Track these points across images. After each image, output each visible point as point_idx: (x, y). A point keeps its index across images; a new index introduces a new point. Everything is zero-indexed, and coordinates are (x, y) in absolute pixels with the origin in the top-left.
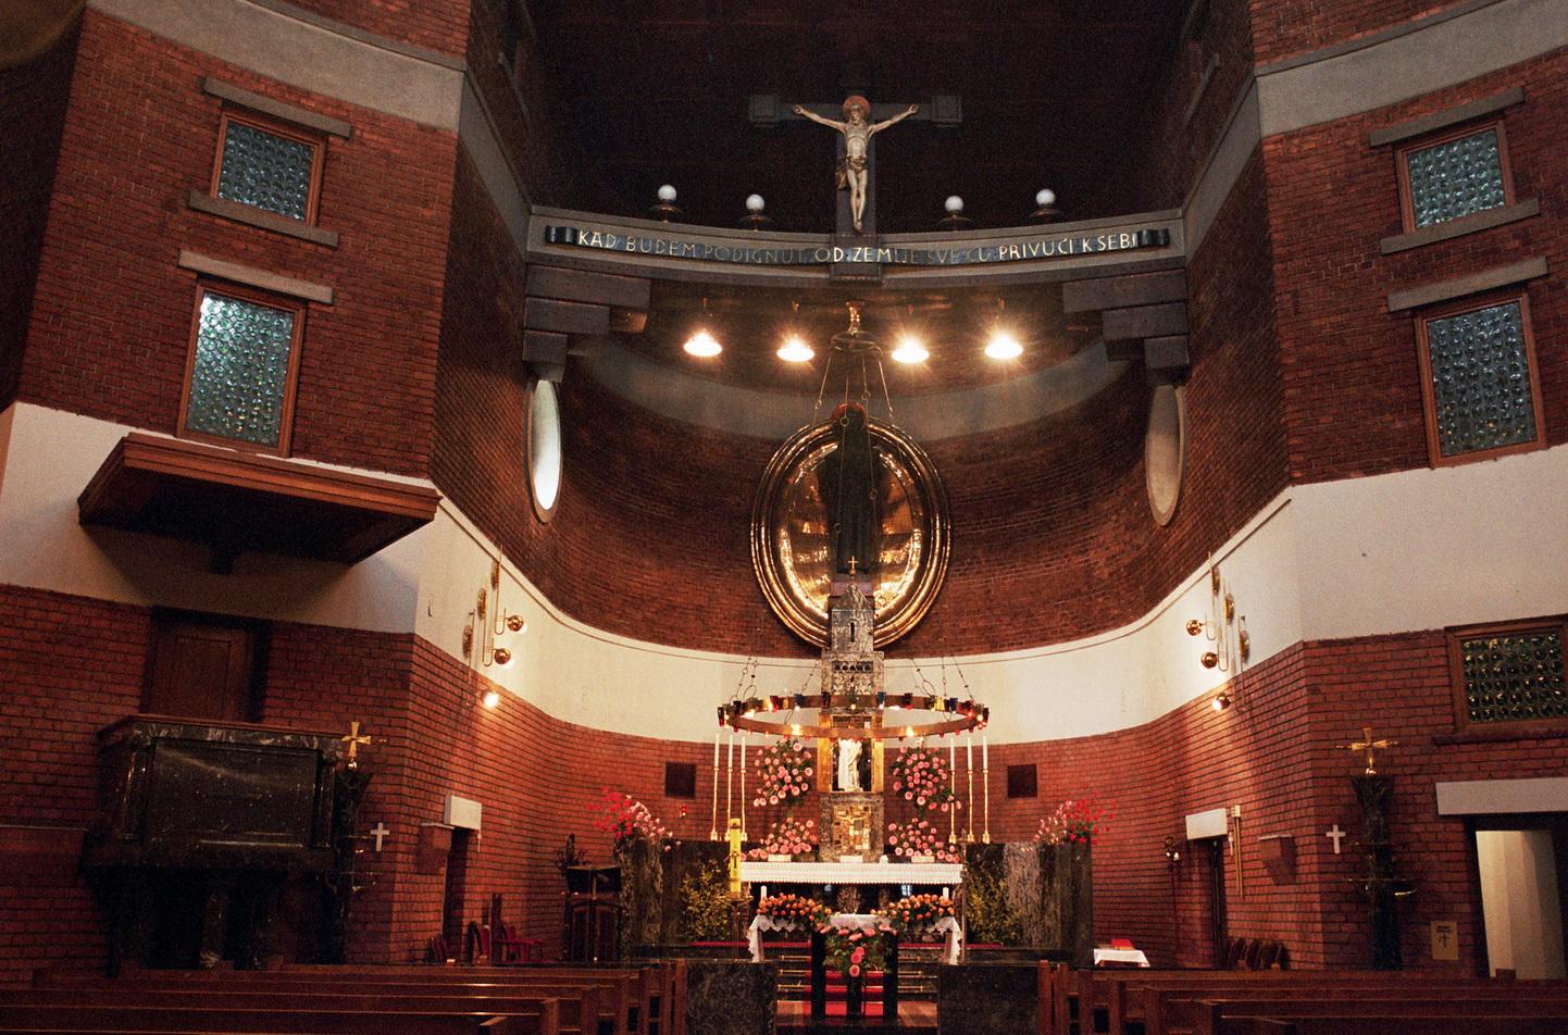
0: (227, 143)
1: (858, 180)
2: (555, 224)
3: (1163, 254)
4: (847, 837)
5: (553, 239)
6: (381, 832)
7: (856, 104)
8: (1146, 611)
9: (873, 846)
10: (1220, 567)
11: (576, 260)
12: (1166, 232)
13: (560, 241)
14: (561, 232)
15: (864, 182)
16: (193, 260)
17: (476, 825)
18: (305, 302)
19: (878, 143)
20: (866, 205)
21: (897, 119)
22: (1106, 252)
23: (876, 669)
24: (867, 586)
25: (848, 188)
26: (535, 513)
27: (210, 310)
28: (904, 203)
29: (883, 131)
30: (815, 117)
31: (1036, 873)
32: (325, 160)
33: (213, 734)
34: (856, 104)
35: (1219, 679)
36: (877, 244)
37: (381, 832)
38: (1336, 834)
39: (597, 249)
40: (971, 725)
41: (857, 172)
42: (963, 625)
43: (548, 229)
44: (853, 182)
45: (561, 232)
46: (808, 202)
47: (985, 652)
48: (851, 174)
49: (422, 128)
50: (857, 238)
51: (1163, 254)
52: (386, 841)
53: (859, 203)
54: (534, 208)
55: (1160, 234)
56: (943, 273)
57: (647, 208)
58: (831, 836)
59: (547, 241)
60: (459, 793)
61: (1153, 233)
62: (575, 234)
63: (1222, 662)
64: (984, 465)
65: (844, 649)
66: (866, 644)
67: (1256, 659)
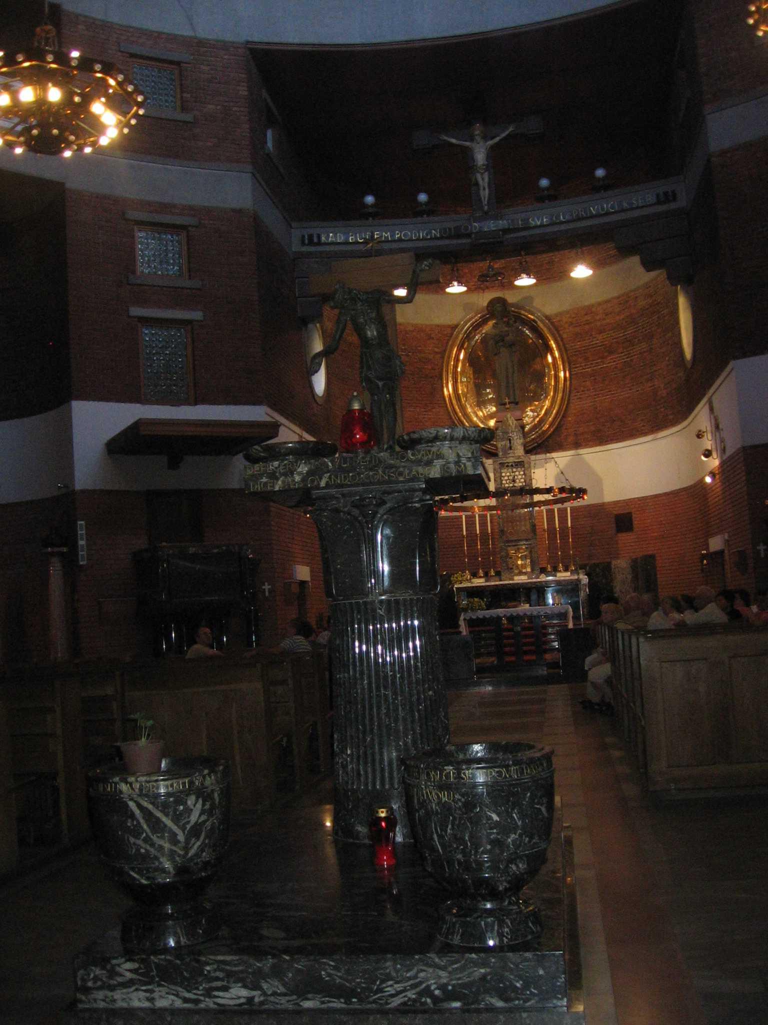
0: (136, 228)
1: (483, 179)
2: (306, 233)
3: (673, 206)
4: (517, 566)
5: (307, 241)
6: (267, 587)
7: (478, 129)
8: (690, 413)
9: (533, 570)
10: (714, 398)
11: (321, 252)
12: (673, 192)
13: (311, 242)
14: (311, 237)
15: (486, 180)
16: (136, 311)
17: (308, 579)
18: (189, 322)
19: (493, 153)
20: (489, 194)
21: (503, 135)
22: (638, 208)
23: (526, 466)
24: (518, 413)
25: (477, 184)
26: (315, 401)
27: (147, 334)
28: (512, 188)
29: (497, 144)
30: (454, 141)
31: (629, 577)
32: (188, 240)
33: (192, 550)
34: (478, 129)
35: (714, 462)
36: (495, 218)
37: (267, 587)
38: (762, 548)
39: (332, 243)
40: (578, 497)
41: (482, 174)
42: (581, 430)
43: (303, 237)
44: (481, 182)
45: (311, 237)
46: (455, 192)
47: (596, 446)
48: (479, 176)
49: (234, 210)
50: (486, 216)
51: (673, 206)
52: (270, 592)
53: (485, 194)
54: (293, 225)
55: (670, 193)
56: (537, 231)
57: (359, 214)
58: (507, 565)
59: (303, 243)
60: (299, 563)
61: (666, 194)
62: (319, 237)
63: (714, 454)
64: (587, 327)
65: (505, 453)
66: (519, 451)
67: (729, 453)
